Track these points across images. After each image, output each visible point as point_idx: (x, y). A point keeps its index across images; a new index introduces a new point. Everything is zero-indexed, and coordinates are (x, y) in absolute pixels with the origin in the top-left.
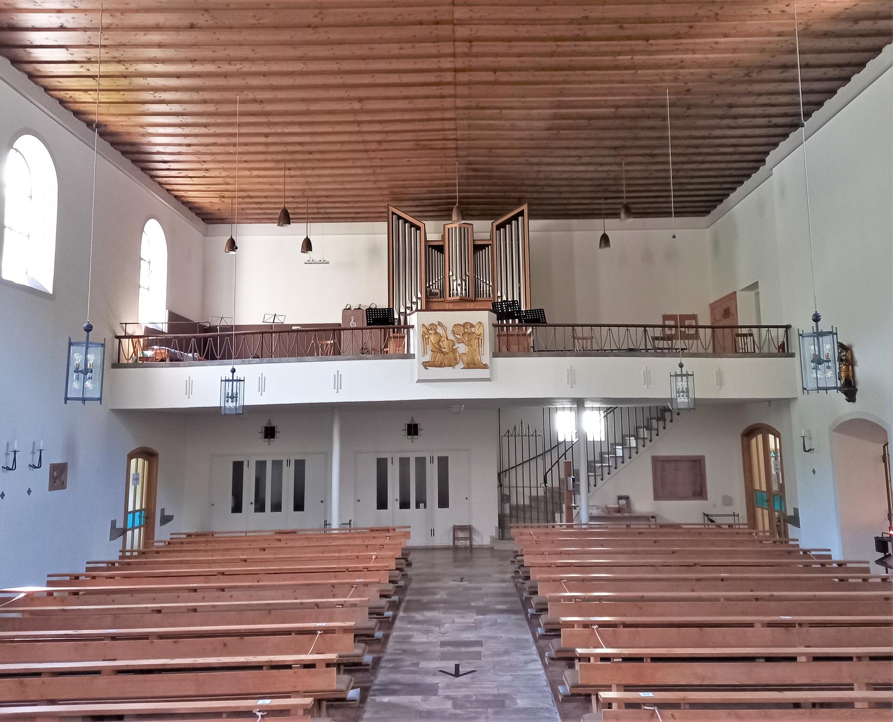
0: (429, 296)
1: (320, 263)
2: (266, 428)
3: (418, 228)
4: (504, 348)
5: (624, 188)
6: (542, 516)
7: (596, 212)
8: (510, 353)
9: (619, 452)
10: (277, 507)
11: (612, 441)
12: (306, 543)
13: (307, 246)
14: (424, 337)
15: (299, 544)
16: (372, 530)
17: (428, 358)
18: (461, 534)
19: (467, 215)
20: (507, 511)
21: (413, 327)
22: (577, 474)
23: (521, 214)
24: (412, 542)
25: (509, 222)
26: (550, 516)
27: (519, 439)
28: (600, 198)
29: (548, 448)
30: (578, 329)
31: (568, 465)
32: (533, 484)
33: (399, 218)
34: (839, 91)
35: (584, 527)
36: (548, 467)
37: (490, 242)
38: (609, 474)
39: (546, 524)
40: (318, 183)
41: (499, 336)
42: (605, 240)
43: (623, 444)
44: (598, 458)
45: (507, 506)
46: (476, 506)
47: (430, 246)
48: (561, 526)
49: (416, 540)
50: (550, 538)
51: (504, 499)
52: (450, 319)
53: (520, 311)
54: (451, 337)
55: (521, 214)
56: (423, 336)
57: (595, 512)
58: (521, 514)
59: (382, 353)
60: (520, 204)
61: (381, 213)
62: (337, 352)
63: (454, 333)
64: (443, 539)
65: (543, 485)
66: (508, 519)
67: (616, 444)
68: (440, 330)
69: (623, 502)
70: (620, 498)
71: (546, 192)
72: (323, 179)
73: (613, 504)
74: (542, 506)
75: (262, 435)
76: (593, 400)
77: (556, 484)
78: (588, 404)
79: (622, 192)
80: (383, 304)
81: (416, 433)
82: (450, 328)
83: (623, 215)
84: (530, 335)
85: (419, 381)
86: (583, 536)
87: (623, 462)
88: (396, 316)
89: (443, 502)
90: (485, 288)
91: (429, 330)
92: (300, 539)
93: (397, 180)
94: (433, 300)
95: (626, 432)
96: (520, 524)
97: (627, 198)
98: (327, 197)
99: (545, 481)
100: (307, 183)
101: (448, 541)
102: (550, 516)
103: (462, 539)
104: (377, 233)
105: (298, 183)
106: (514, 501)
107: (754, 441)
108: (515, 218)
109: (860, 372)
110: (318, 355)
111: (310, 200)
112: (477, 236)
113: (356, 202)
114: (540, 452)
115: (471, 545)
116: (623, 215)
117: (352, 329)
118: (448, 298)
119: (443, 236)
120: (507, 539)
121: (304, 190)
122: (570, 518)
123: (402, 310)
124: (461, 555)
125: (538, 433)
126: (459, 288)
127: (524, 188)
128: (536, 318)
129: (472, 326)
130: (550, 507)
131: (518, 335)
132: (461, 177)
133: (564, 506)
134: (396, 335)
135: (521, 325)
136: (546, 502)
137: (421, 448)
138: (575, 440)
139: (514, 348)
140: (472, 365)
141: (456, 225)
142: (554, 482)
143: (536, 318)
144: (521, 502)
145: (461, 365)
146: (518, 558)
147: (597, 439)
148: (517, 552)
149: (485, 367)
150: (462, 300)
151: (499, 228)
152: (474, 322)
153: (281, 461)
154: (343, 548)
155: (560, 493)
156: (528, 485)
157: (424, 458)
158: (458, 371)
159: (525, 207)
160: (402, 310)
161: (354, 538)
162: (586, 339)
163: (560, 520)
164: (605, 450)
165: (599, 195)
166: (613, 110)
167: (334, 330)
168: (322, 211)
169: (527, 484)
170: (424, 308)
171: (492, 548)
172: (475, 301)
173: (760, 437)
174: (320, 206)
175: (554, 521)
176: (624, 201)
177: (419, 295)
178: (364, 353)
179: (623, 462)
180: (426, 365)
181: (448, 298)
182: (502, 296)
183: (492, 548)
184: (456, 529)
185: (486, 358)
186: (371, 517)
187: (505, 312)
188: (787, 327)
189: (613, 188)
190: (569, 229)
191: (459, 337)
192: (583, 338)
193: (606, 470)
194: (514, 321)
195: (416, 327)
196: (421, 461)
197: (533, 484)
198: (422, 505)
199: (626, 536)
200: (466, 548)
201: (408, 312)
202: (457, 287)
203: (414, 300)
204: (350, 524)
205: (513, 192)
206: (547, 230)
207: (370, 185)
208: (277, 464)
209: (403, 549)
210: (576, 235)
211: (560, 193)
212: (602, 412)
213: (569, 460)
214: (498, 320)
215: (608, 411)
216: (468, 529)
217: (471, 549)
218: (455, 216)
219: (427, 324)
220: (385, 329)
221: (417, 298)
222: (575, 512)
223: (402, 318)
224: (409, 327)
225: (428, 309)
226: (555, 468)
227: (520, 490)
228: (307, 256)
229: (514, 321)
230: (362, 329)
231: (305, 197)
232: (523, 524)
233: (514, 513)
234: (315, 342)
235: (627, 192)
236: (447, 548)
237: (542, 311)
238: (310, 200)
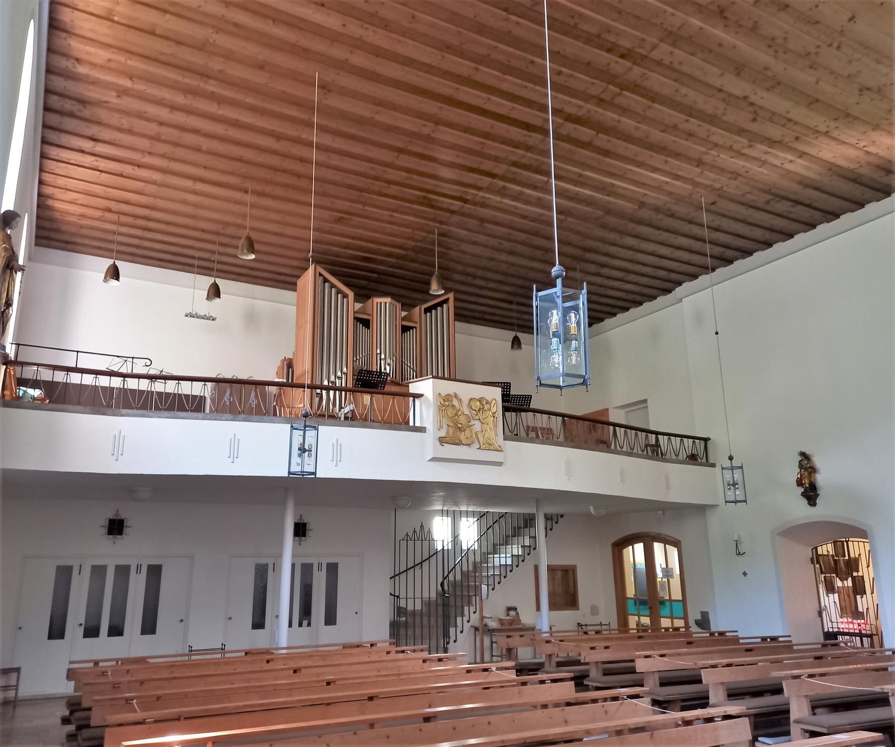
1: (203, 317)
7: (487, 317)
10: (116, 631)
17: (443, 433)
29: (426, 556)
34: (797, 237)
44: (471, 568)
54: (467, 412)
67: (488, 554)
68: (455, 402)
69: (512, 613)
70: (509, 609)
74: (418, 620)
75: (105, 530)
82: (465, 402)
85: (434, 459)
107: (625, 551)
109: (820, 479)
114: (418, 560)
157: (311, 565)
164: (478, 559)
166: (600, 213)
169: (410, 595)
173: (639, 547)
177: (345, 369)
180: (442, 441)
188: (706, 440)
198: (305, 623)
203: (339, 374)
208: (123, 572)
219: (443, 394)
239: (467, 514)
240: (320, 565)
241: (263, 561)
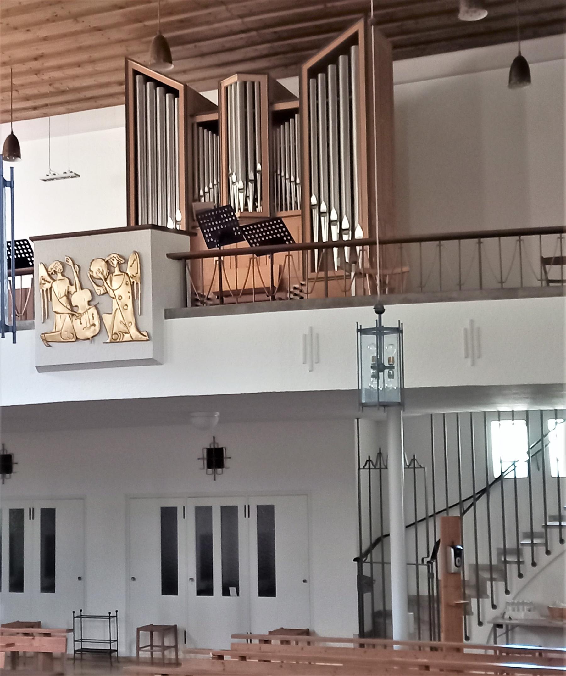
2: (210, 451)
23: (354, 40)
25: (332, 59)
60: (352, 22)
75: (202, 464)
89: (267, 588)
108: (344, 49)
153: (175, 509)
196: (229, 514)
198: (232, 590)
208: (229, 514)
240: (247, 509)
241: (170, 504)
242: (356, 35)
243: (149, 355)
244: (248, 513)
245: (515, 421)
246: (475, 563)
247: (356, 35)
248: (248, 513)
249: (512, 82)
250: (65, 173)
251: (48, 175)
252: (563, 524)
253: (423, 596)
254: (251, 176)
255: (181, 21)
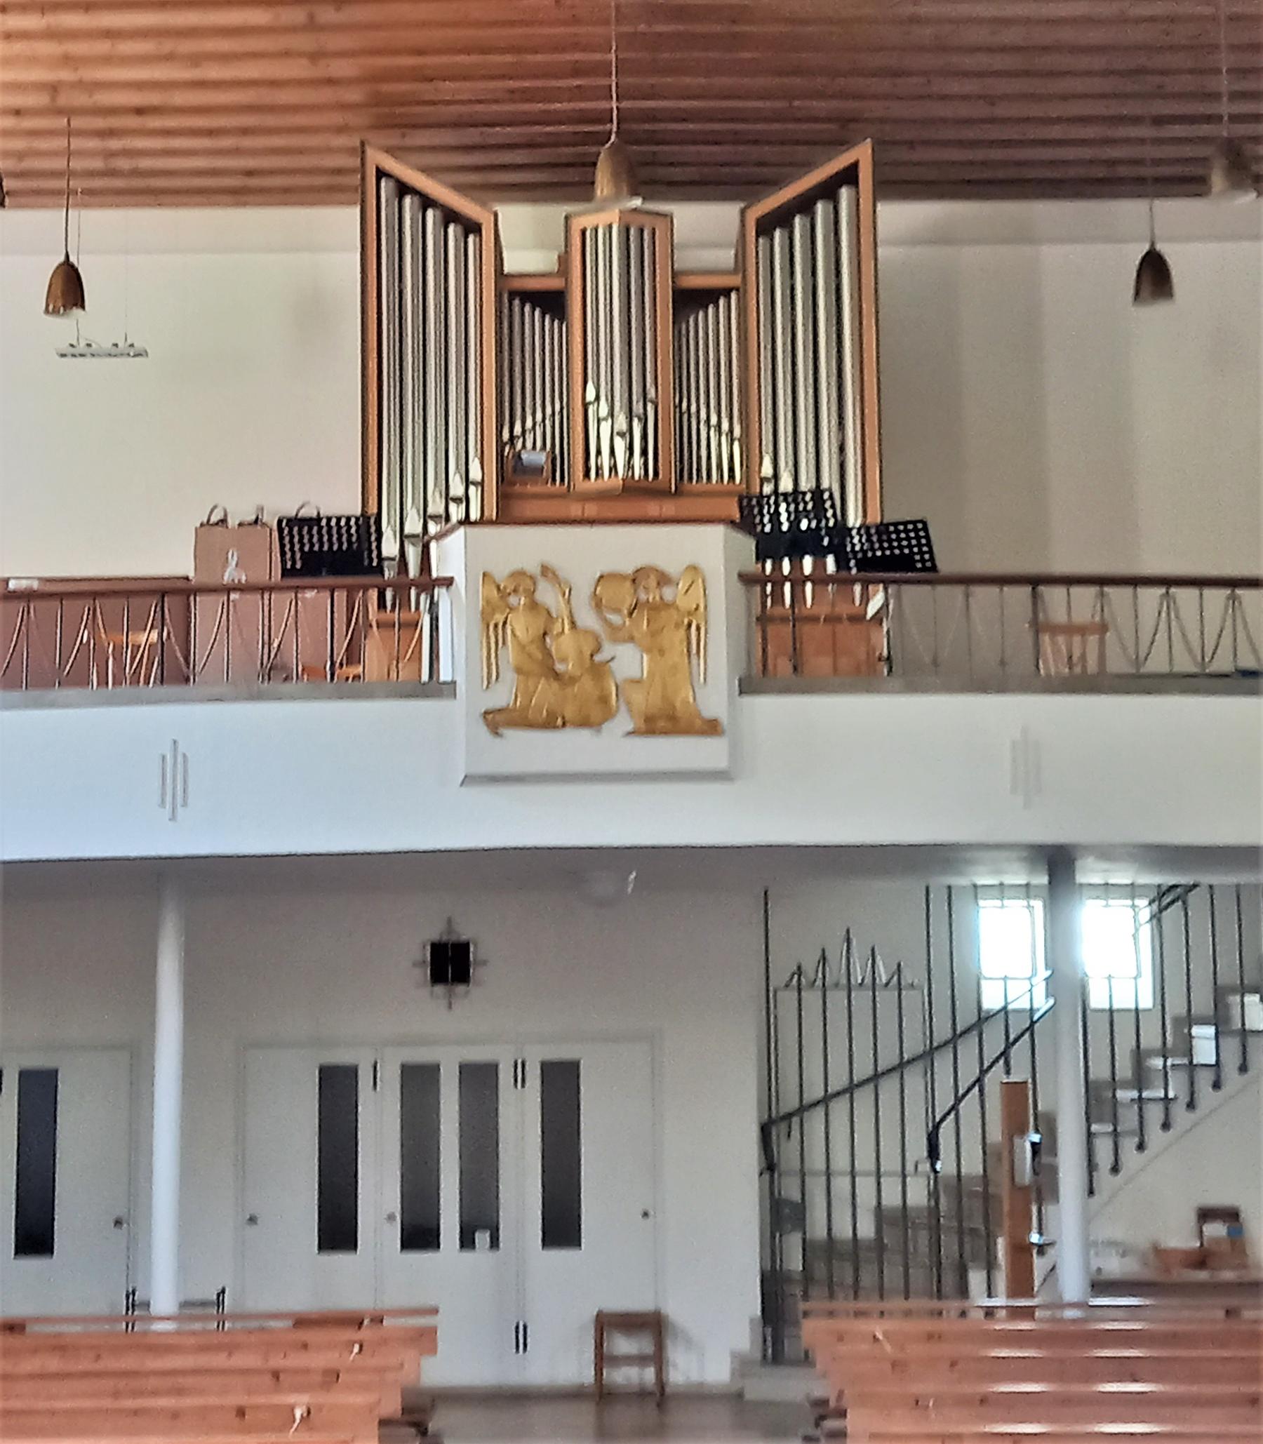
0: (511, 473)
3: (471, 228)
4: (783, 666)
5: (1224, 84)
6: (918, 1276)
7: (1123, 171)
8: (800, 678)
9: (1205, 1051)
11: (1176, 1007)
12: (53, 1364)
13: (69, 288)
14: (492, 619)
15: (30, 1365)
16: (302, 1322)
17: (503, 695)
18: (623, 1345)
19: (653, 182)
20: (795, 1263)
21: (448, 582)
22: (1048, 1125)
23: (850, 176)
24: (443, 1369)
25: (805, 204)
26: (949, 1279)
27: (837, 999)
28: (1136, 120)
30: (1054, 596)
31: (1017, 1096)
32: (890, 1162)
33: (403, 189)
35: (1070, 1314)
36: (944, 1100)
37: (735, 280)
38: (1166, 1126)
39: (935, 1304)
40: (107, 60)
41: (763, 620)
42: (1154, 275)
43: (1219, 1019)
44: (1125, 1069)
45: (793, 1243)
46: (681, 1239)
47: (513, 294)
48: (990, 1312)
49: (453, 1365)
50: (946, 1350)
51: (781, 1215)
52: (588, 553)
53: (841, 530)
54: (588, 618)
55: (850, 176)
56: (486, 617)
57: (1114, 1266)
58: (845, 1273)
59: (338, 672)
60: (844, 143)
61: (339, 171)
62: (174, 671)
63: (598, 603)
64: (563, 1361)
65: (926, 1166)
66: (798, 1292)
68: (547, 595)
69: (1216, 1230)
70: (1206, 1215)
71: (944, 98)
72: (127, 47)
73: (1181, 1237)
76: (1107, 853)
77: (973, 1165)
78: (1089, 873)
79: (1215, 96)
80: (340, 499)
81: (462, 976)
83: (1218, 180)
84: (878, 618)
85: (468, 780)
86: (1070, 1349)
87: (1217, 1085)
88: (390, 547)
89: (561, 1227)
90: (719, 447)
91: (506, 595)
92: (35, 1351)
93: (396, 52)
94: (519, 491)
95: (1229, 975)
96: (840, 1304)
97: (1234, 118)
98: (140, 111)
99: (933, 1153)
100: (67, 60)
101: (576, 1368)
102: (949, 1279)
103: (629, 1360)
104: (324, 245)
105: (33, 61)
106: (818, 1230)
108: (828, 190)
110: (103, 682)
111: (77, 123)
112: (687, 259)
113: (245, 131)
115: (661, 1382)
116: (1218, 180)
117: (228, 590)
118: (580, 484)
119: (564, 260)
120: (795, 1363)
121: (54, 88)
122: (1021, 1283)
123: (413, 525)
124: (624, 1416)
125: (907, 977)
126: (620, 445)
127: (859, 83)
128: (899, 554)
129: (664, 579)
130: (949, 1246)
131: (832, 619)
132: (627, 41)
133: (1001, 1244)
134: (388, 615)
135: (849, 578)
136: (935, 1229)
137: (489, 1027)
138: (1042, 1003)
139: (820, 663)
140: (664, 721)
141: (612, 216)
142: (965, 1157)
143: (899, 554)
144: (843, 1230)
145: (623, 722)
146: (831, 1424)
147: (1124, 1001)
148: (823, 1402)
149: (712, 728)
150: (630, 490)
151: (765, 227)
152: (673, 567)
154: (188, 1381)
155: (986, 1197)
156: (870, 1169)
157: (490, 1070)
158: (614, 745)
159: (862, 153)
160: (413, 525)
161: (231, 1349)
162: (1082, 630)
163: (987, 1293)
164: (1151, 1039)
165: (1127, 109)
167: (171, 596)
168: (123, 164)
169: (865, 1161)
170: (492, 512)
171: (740, 1395)
172: (678, 493)
174: (114, 144)
175: (963, 1291)
176: (1224, 131)
177: (475, 474)
178: (273, 674)
179: (1217, 1085)
180: (496, 720)
181: (580, 484)
182: (776, 476)
183: (740, 1395)
184: (605, 1324)
185: (713, 690)
186: (299, 1277)
187: (787, 535)
189: (1185, 83)
190: (1024, 236)
191: (615, 618)
192: (1070, 629)
193: (1154, 1114)
194: (819, 565)
195: (460, 581)
197: (890, 1162)
198: (482, 1238)
199: (1224, 1345)
200: (641, 1394)
201: (433, 528)
202: (614, 445)
203: (457, 489)
204: (219, 1302)
205: (821, 95)
206: (941, 237)
207: (297, 69)
208: (480, 1080)
209: (405, 1393)
210: (1053, 255)
211: (991, 100)
212: (1142, 903)
213: (1020, 1074)
214: (761, 557)
215: (1164, 898)
216: (652, 1325)
217: (660, 1397)
218: (603, 183)
220: (351, 591)
221: (468, 482)
222: (1039, 1265)
223: (413, 554)
224: (429, 583)
225: (505, 515)
226: (970, 1106)
227: (841, 1185)
228: (68, 326)
229: (819, 565)
230: (262, 589)
231: (60, 112)
232: (852, 1305)
233: (820, 1270)
234: (94, 634)
235: (1235, 96)
236: (572, 1395)
237: (920, 528)
238: (77, 123)
239: (1001, 890)
240: (520, 1068)
241: (342, 1057)
242: (854, 166)
243: (722, 763)
244: (520, 1077)
245: (1006, 902)
246: (955, 1172)
247: (854, 166)
248: (520, 1077)
249: (1146, 291)
250: (116, 345)
251: (72, 346)
252: (1145, 1094)
253: (843, 1242)
254: (638, 408)
255: (524, 90)
